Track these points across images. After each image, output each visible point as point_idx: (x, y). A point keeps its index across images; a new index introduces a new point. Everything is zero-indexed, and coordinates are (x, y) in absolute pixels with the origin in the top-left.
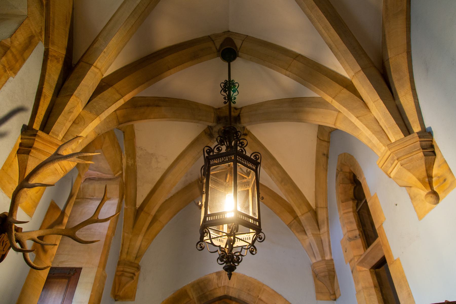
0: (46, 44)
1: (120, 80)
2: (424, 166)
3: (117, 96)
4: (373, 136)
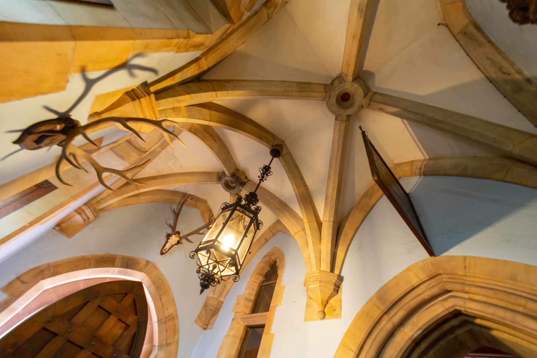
0: (203, 55)
1: (216, 111)
2: (329, 295)
3: (208, 118)
4: (314, 258)
